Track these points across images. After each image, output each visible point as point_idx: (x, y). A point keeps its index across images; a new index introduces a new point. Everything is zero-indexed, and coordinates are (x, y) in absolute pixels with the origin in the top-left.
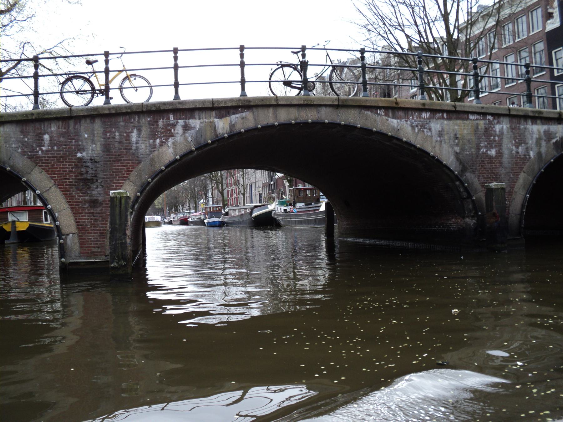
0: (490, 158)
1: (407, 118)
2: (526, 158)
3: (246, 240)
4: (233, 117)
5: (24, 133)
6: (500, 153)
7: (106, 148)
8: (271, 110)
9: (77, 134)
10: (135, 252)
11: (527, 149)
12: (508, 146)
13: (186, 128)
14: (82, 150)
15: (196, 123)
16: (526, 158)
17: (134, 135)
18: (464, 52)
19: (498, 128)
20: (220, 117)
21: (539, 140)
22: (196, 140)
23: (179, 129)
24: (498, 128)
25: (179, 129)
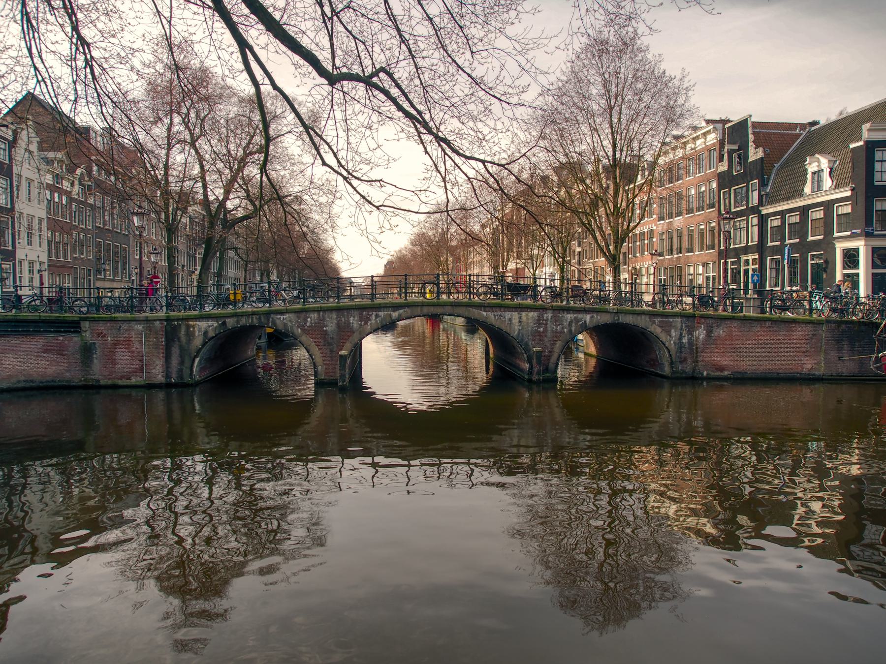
0: (540, 332)
1: (492, 311)
2: (562, 332)
3: (527, 447)
4: (401, 311)
5: (299, 318)
6: (545, 330)
7: (338, 325)
8: (419, 308)
9: (324, 318)
10: (44, 107)
11: (563, 328)
12: (551, 326)
13: (377, 316)
14: (326, 326)
15: (381, 314)
16: (562, 332)
17: (351, 319)
18: (26, 314)
19: (545, 316)
20: (394, 311)
21: (571, 322)
22: (381, 322)
23: (373, 317)
24: (545, 316)
25: (373, 317)
